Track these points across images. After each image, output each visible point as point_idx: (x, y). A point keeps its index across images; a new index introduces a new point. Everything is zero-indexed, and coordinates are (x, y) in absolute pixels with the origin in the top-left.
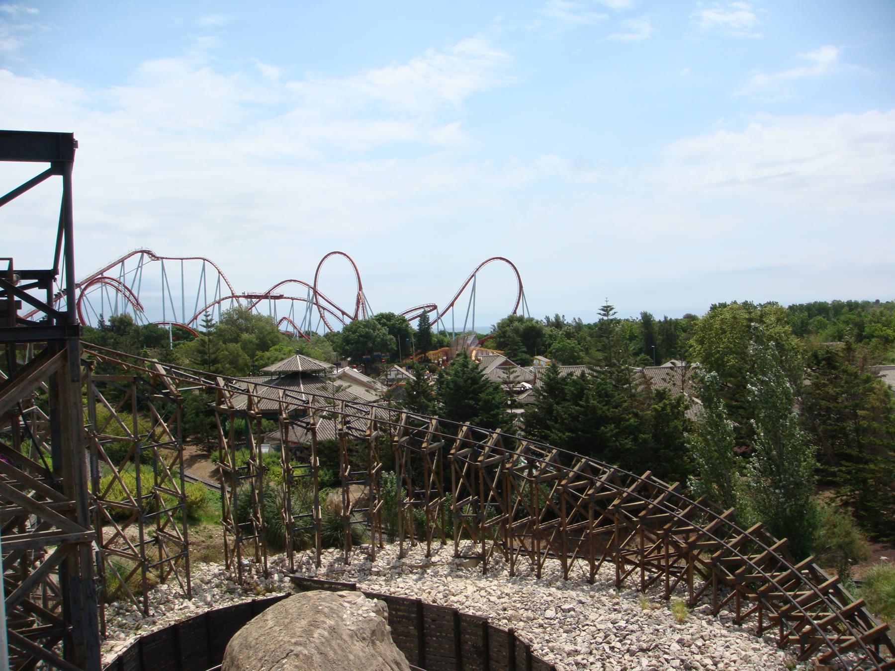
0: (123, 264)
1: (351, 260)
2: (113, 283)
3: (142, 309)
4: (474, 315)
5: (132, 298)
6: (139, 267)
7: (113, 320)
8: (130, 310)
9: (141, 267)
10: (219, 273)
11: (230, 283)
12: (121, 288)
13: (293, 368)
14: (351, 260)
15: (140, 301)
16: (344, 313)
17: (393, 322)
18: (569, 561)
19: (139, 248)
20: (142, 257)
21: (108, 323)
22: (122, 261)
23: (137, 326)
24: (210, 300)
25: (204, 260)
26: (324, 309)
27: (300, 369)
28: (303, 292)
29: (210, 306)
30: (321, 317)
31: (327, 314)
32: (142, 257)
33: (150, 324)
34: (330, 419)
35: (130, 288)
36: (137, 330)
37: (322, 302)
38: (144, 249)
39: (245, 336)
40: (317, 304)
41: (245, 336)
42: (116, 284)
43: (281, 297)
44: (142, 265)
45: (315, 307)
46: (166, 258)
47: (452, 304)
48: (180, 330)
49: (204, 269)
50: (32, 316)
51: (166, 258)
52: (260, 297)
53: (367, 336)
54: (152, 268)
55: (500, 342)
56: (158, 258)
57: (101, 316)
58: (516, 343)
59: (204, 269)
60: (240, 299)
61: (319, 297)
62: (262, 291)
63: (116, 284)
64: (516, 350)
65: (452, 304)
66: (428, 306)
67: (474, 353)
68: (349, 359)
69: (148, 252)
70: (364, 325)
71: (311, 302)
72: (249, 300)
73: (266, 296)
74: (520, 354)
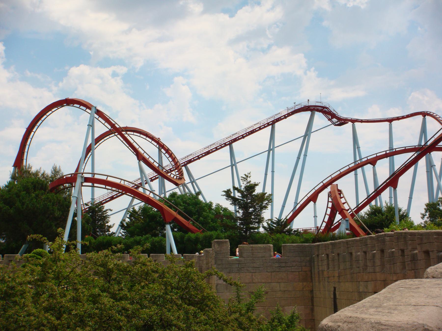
22: (273, 123)
46: (362, 121)
51: (362, 121)
56: (342, 122)
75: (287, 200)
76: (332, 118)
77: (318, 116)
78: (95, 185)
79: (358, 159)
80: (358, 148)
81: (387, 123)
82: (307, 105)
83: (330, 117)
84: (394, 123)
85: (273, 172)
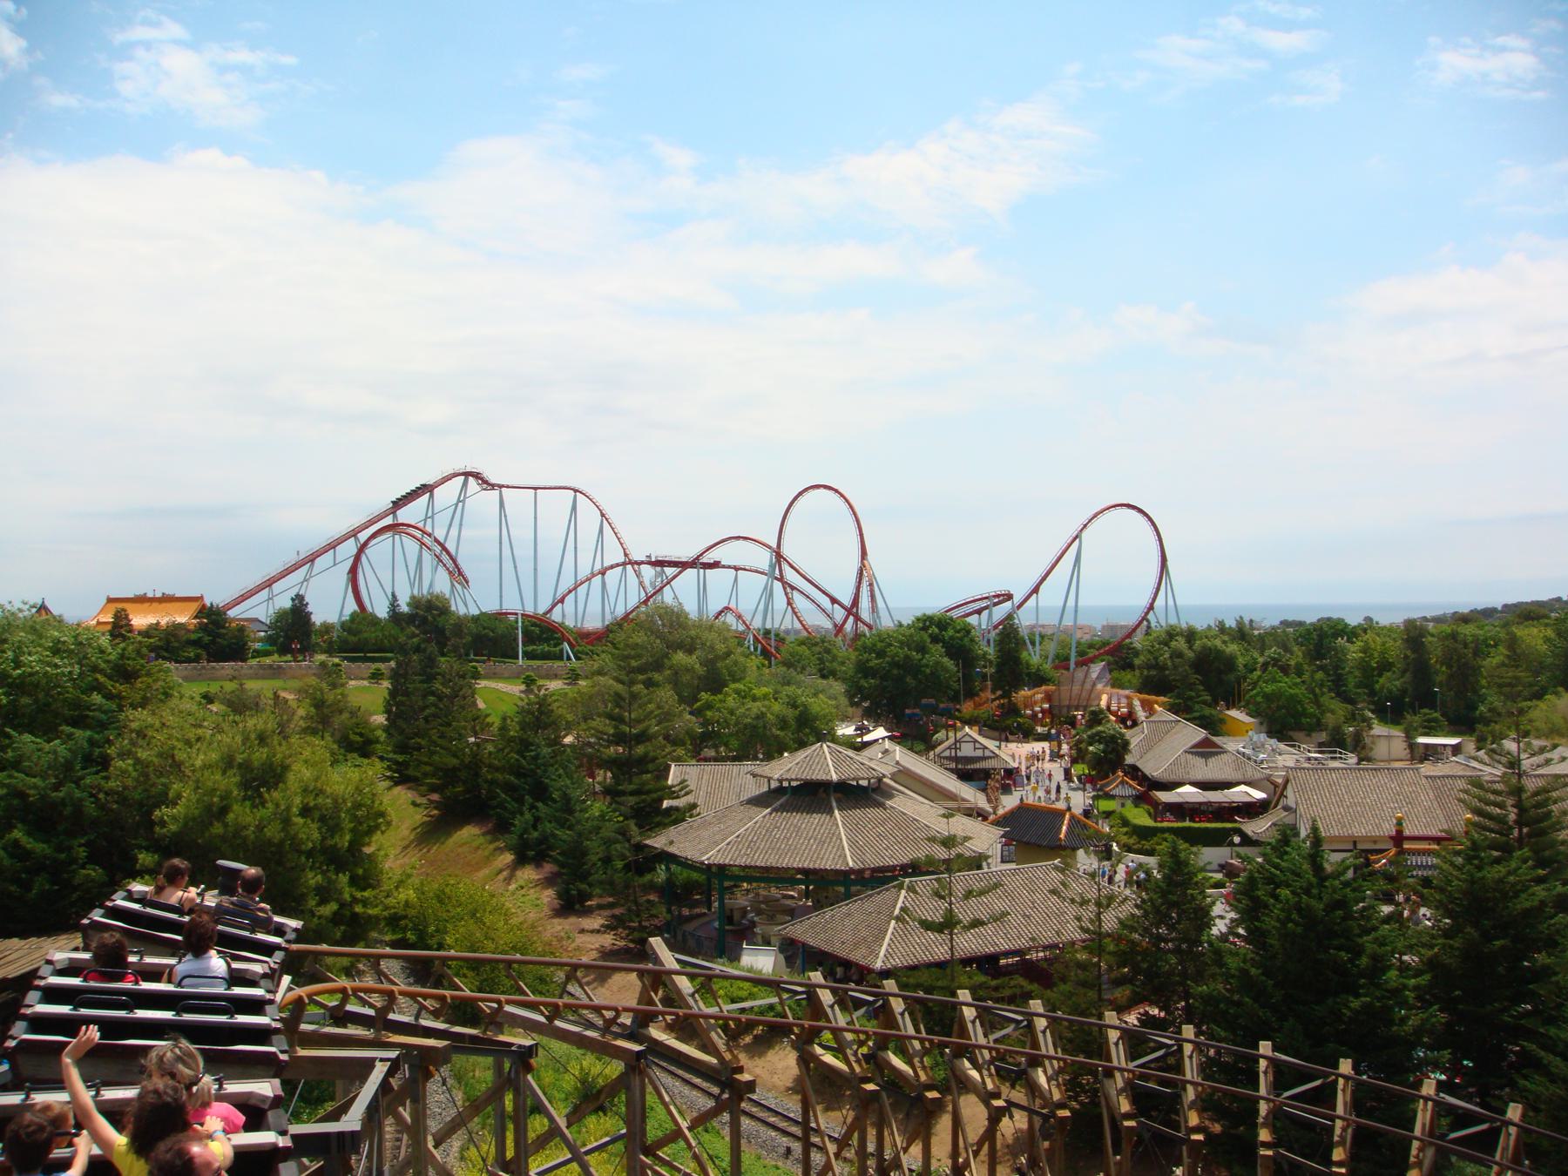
2: (411, 530)
3: (467, 582)
5: (445, 557)
6: (459, 501)
7: (415, 602)
8: (441, 584)
9: (463, 501)
11: (622, 534)
12: (427, 540)
13: (818, 775)
15: (460, 561)
16: (834, 601)
17: (951, 632)
19: (460, 467)
20: (465, 484)
21: (404, 608)
23: (459, 617)
24: (584, 572)
25: (576, 491)
26: (793, 588)
27: (835, 777)
28: (763, 559)
29: (582, 583)
30: (789, 603)
31: (796, 596)
32: (465, 484)
33: (483, 614)
34: (940, 931)
35: (442, 541)
36: (461, 624)
37: (790, 575)
39: (680, 657)
40: (781, 579)
41: (680, 657)
42: (418, 534)
43: (716, 565)
45: (778, 585)
46: (508, 487)
47: (1036, 590)
48: (534, 625)
49: (574, 508)
50: (270, 585)
51: (508, 487)
52: (683, 565)
53: (907, 666)
54: (482, 502)
55: (1147, 677)
56: (493, 486)
57: (393, 595)
58: (1191, 687)
59: (574, 508)
60: (642, 566)
61: (785, 567)
62: (686, 554)
63: (418, 534)
64: (1191, 698)
65: (1036, 590)
66: (998, 596)
67: (1105, 698)
68: (866, 704)
69: (477, 476)
70: (902, 643)
71: (769, 574)
72: (658, 569)
73: (693, 563)
74: (1197, 707)
81: (533, 491)
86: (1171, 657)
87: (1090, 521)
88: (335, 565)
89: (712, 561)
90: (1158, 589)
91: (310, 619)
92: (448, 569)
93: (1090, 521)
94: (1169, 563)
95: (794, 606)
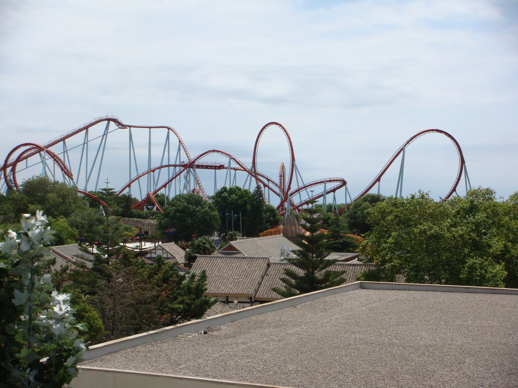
0: (87, 133)
1: (285, 131)
2: (59, 162)
4: (87, 156)
6: (104, 134)
10: (180, 142)
14: (285, 131)
18: (93, 262)
22: (86, 128)
38: (110, 117)
44: (107, 133)
46: (135, 127)
47: (378, 179)
51: (135, 127)
56: (123, 126)
65: (378, 179)
69: (115, 121)
75: (102, 346)
76: (119, 125)
77: (112, 123)
78: (306, 188)
79: (469, 188)
80: (132, 143)
81: (149, 129)
82: (106, 118)
83: (118, 124)
84: (152, 129)
85: (299, 174)
86: (429, 214)
87: (408, 142)
88: (27, 168)
89: (219, 165)
90: (459, 179)
91: (131, 198)
92: (61, 167)
93: (408, 142)
94: (467, 164)
95: (201, 185)
